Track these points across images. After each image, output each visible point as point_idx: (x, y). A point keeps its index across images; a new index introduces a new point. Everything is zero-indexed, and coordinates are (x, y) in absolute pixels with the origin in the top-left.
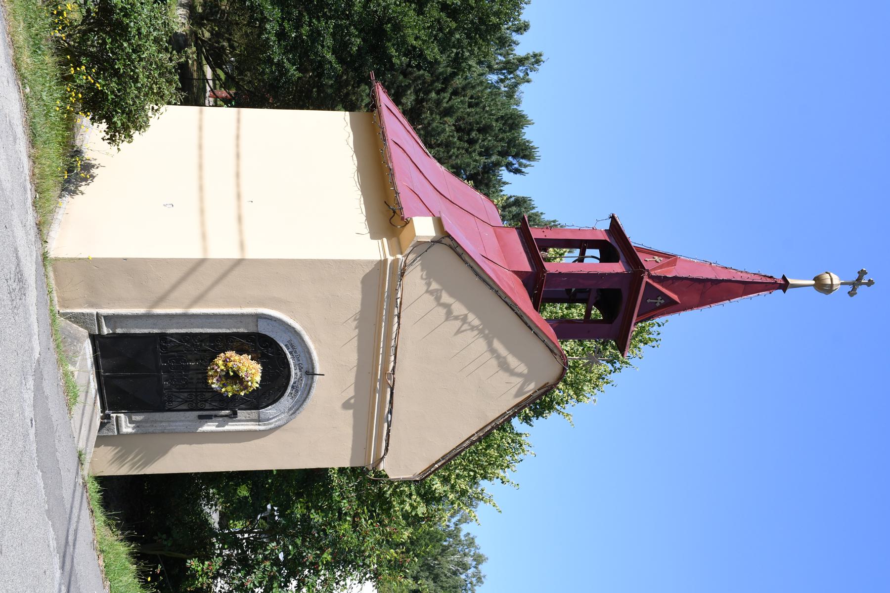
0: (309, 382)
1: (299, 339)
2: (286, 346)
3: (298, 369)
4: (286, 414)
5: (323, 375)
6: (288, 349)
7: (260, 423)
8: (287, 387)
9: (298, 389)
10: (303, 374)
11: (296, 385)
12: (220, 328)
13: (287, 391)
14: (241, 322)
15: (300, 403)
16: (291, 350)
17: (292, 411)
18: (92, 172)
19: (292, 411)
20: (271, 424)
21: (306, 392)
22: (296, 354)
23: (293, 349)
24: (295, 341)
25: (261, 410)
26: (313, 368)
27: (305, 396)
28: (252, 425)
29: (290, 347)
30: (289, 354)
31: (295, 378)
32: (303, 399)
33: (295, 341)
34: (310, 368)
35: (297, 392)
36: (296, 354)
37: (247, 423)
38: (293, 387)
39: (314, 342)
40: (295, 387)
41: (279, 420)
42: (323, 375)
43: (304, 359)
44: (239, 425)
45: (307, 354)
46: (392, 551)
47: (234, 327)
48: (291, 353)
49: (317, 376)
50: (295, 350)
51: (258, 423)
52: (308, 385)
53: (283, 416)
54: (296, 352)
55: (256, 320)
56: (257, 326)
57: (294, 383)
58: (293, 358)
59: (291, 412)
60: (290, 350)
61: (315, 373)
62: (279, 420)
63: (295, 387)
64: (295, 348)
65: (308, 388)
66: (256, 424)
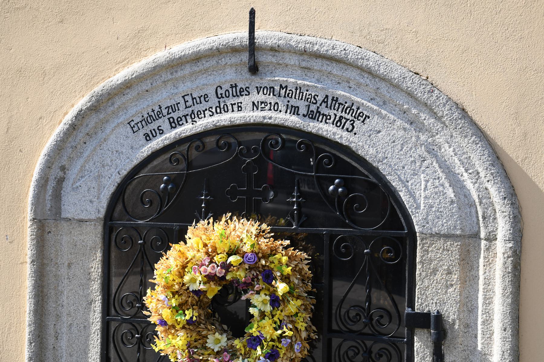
0: (293, 60)
1: (124, 99)
2: (148, 138)
3: (236, 100)
4: (440, 139)
5: (252, 13)
6: (162, 132)
7: (483, 235)
8: (310, 134)
9: (320, 98)
10: (257, 81)
11: (302, 106)
12: (87, 328)
13: (330, 136)
14: (69, 266)
15: (384, 88)
16: (164, 123)
17: (423, 116)
18: (181, 333)
19: (423, 116)
20: (485, 195)
21: (336, 70)
22: (182, 106)
23: (159, 115)
24: (132, 111)
25: (417, 229)
26: (234, 50)
27: (352, 74)
28: (489, 263)
29: (154, 126)
30: (179, 130)
31: (275, 107)
32: (366, 80)
33: (132, 111)
34: (234, 59)
35: (335, 100)
36: (182, 106)
37: (481, 282)
38: (312, 116)
39: (139, 53)
40: (313, 108)
41: (468, 166)
42: (252, 13)
43: (202, 80)
44: (488, 313)
45: (180, 74)
46: (428, 354)
47: (86, 286)
48: (174, 124)
49: (258, 33)
50: (165, 112)
51: (483, 243)
52: (304, 64)
53: (447, 151)
54: (173, 108)
55: (65, 224)
56: (81, 221)
57: (295, 110)
58: (194, 116)
59: (429, 121)
60: (165, 125)
61: (246, 41)
62: (468, 166)
63: (313, 108)
64: (157, 109)
65: (317, 64)
66: (488, 249)
